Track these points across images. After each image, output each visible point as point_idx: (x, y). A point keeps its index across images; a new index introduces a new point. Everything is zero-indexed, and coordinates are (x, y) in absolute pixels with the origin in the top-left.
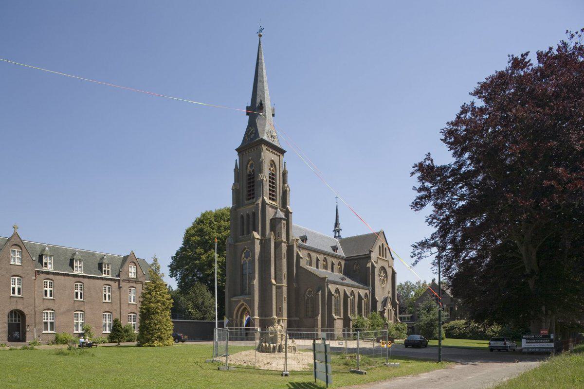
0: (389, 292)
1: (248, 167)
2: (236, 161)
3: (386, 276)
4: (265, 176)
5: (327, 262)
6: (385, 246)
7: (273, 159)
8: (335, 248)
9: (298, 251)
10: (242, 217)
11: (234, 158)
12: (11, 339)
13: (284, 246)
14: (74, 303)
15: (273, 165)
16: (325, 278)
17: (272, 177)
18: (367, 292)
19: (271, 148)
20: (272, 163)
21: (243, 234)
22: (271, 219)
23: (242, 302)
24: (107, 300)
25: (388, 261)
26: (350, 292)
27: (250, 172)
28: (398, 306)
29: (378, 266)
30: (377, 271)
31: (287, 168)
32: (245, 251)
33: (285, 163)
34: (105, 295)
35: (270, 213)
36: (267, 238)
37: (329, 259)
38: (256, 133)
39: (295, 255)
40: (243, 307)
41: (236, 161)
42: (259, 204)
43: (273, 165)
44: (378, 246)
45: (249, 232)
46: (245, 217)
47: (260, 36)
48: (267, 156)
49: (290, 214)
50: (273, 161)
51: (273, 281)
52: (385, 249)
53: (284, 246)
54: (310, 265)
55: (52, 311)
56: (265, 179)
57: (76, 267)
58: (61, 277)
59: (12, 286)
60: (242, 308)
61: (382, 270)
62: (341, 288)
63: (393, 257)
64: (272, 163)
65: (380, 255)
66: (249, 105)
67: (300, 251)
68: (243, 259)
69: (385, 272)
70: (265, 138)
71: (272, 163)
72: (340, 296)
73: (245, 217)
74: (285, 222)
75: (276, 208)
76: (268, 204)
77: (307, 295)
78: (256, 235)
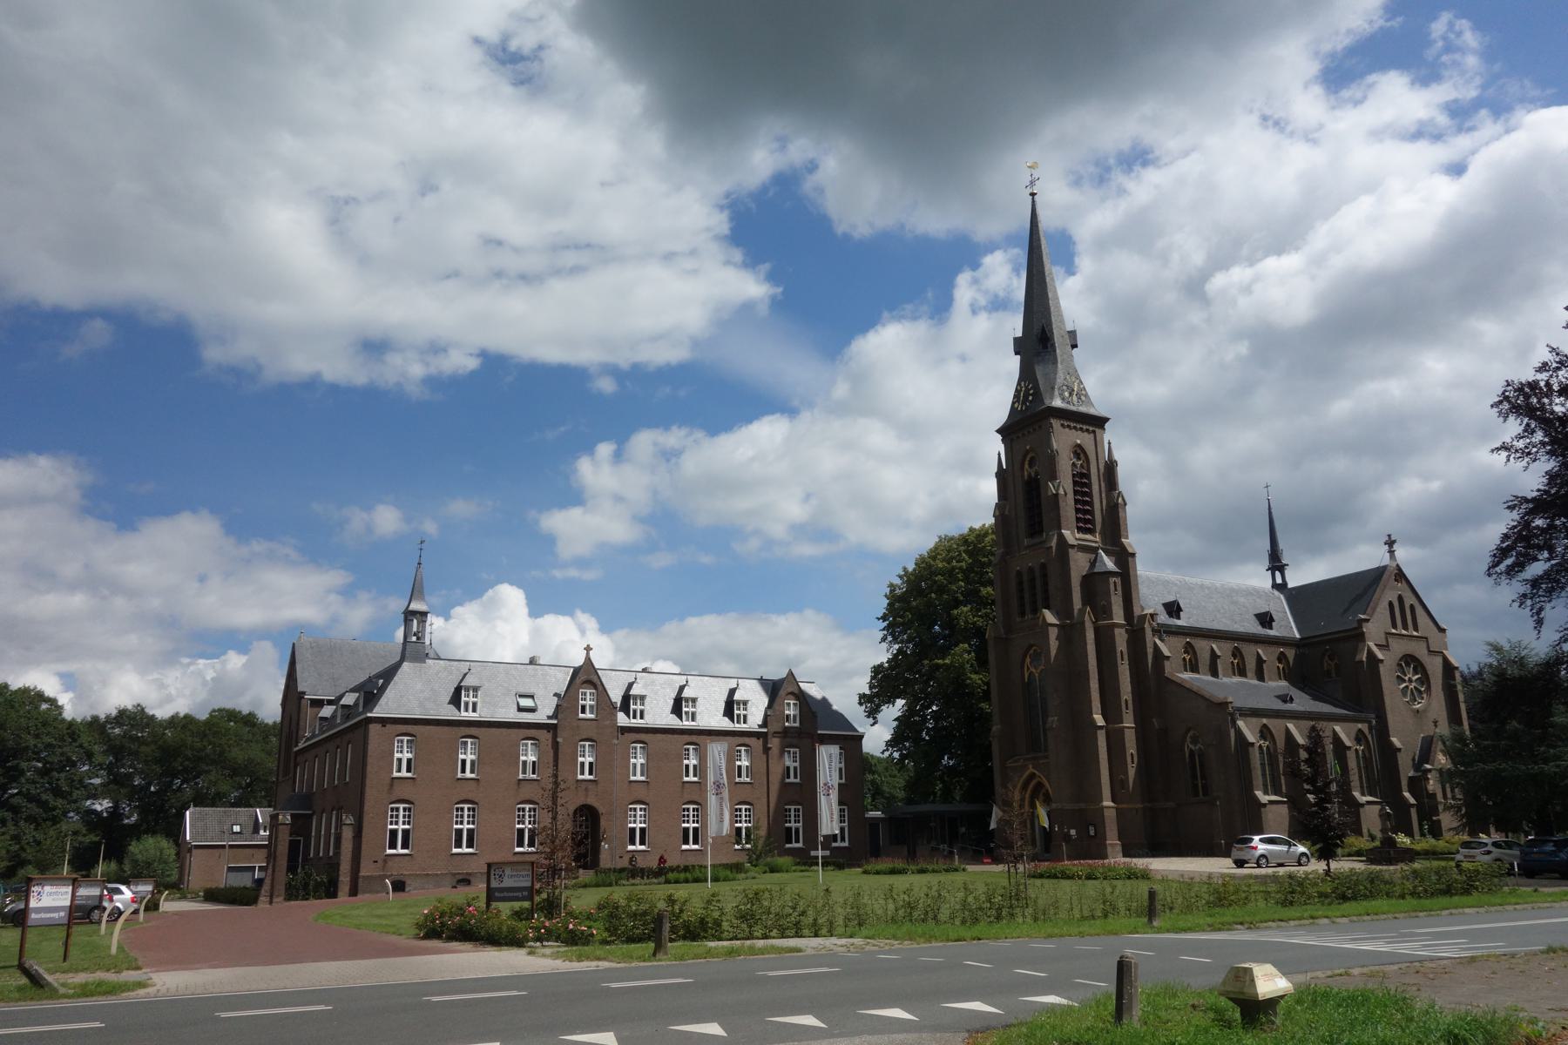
0: (1435, 723)
1: (1026, 466)
2: (999, 454)
3: (1425, 680)
4: (1064, 485)
5: (1242, 658)
6: (1409, 600)
7: (1079, 442)
8: (1265, 619)
9: (1158, 642)
10: (1019, 574)
11: (994, 449)
12: (403, 890)
13: (1121, 639)
14: (683, 787)
15: (1082, 455)
16: (1227, 703)
17: (1081, 481)
18: (1364, 727)
19: (1078, 422)
20: (1079, 451)
21: (1023, 614)
22: (1084, 576)
23: (1031, 770)
24: (468, 774)
25: (1426, 638)
26: (1353, 735)
27: (1029, 475)
28: (1413, 811)
29: (1388, 660)
30: (1387, 674)
31: (1116, 456)
32: (1032, 652)
33: (1109, 443)
34: (464, 762)
35: (1079, 564)
36: (1075, 621)
37: (1250, 651)
38: (1038, 395)
39: (1150, 651)
40: (1034, 783)
41: (999, 454)
42: (1051, 547)
43: (1082, 455)
44: (1384, 605)
45: (1036, 611)
46: (1025, 578)
47: (1033, 195)
48: (1063, 439)
49: (1130, 559)
50: (1079, 446)
51: (1099, 720)
52: (1412, 607)
53: (1121, 639)
54: (1194, 668)
55: (644, 806)
56: (1061, 492)
57: (687, 713)
58: (659, 736)
59: (397, 755)
60: (1031, 786)
61: (1408, 665)
62: (1275, 725)
63: (1443, 626)
64: (1079, 451)
65: (1394, 626)
66: (1019, 334)
67: (1162, 641)
68: (1028, 669)
69: (1419, 667)
70: (1057, 403)
71: (1079, 451)
72: (1275, 743)
73: (1025, 578)
74: (1118, 580)
75: (1094, 550)
76: (1073, 546)
77: (1189, 746)
78: (1050, 617)
